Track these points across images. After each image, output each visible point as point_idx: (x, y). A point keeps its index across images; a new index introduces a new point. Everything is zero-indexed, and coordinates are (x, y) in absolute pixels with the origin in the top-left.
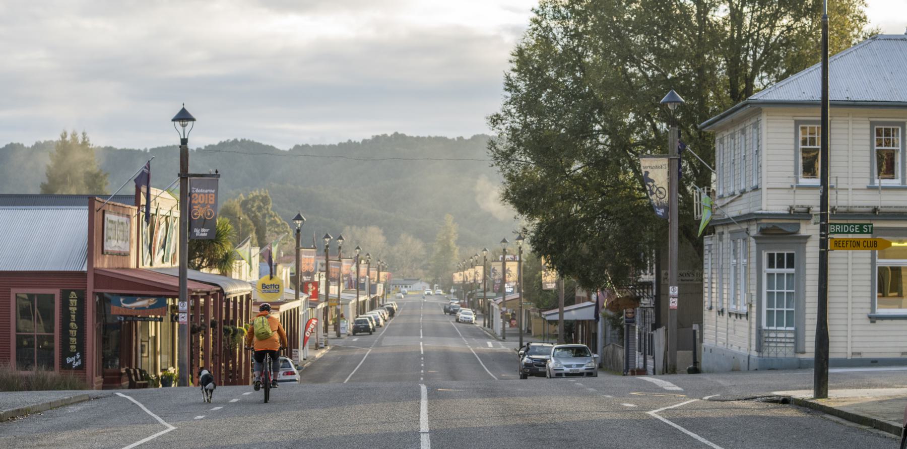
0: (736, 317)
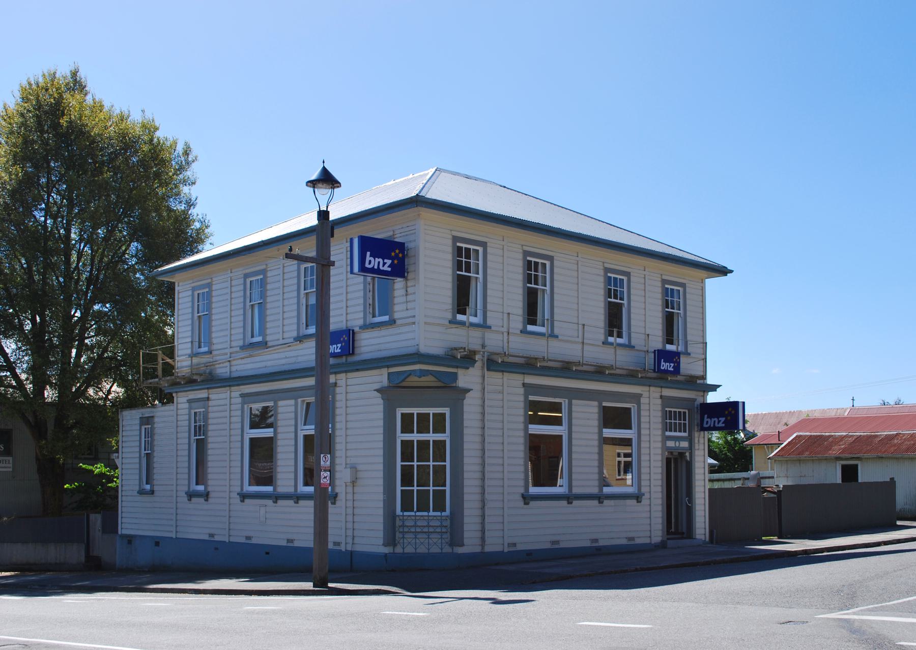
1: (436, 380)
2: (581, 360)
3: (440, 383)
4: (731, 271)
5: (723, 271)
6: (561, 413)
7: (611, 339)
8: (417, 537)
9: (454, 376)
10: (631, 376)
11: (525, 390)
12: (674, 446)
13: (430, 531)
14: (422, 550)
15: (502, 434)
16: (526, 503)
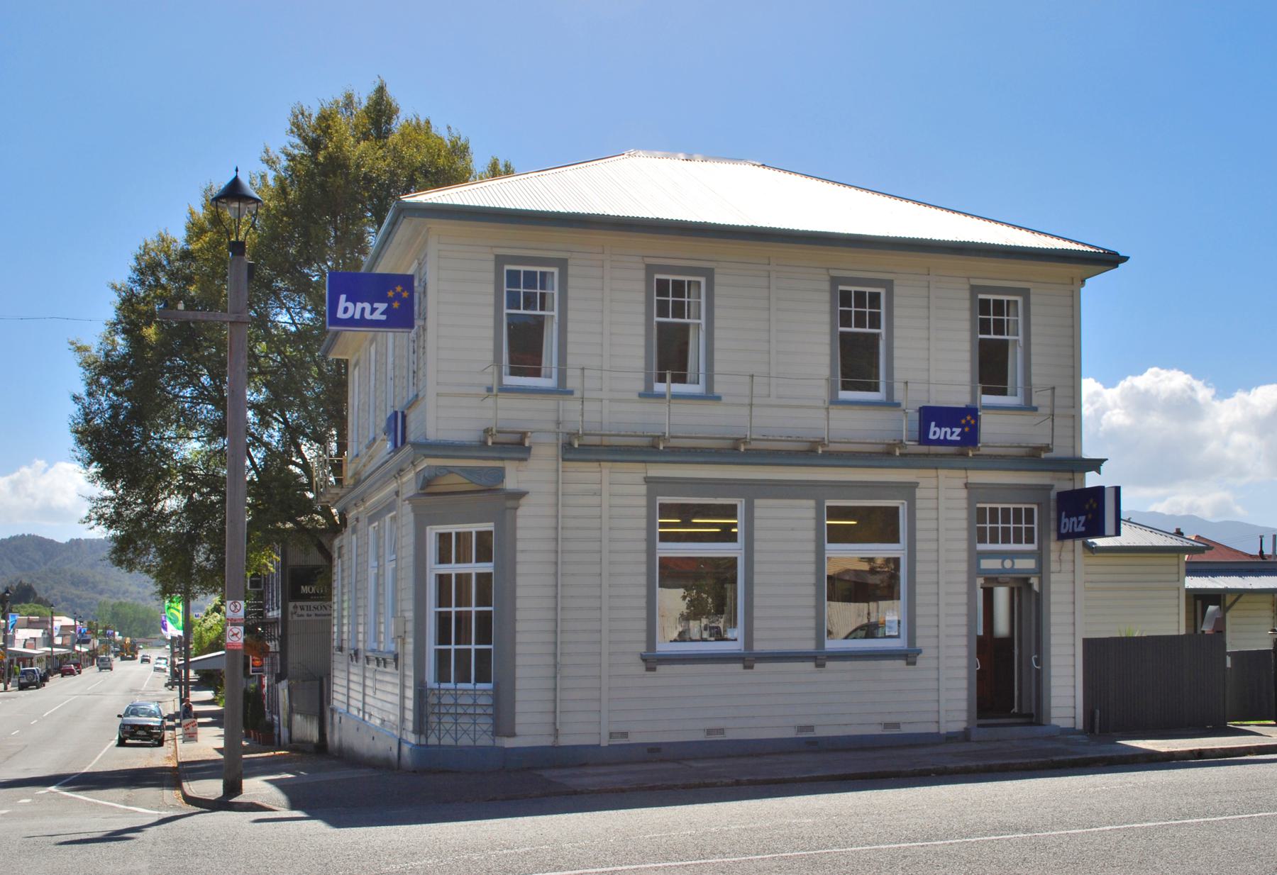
0: (378, 665)
1: (467, 481)
2: (748, 434)
3: (473, 485)
4: (1125, 259)
5: (1110, 260)
6: (736, 519)
7: (659, 387)
8: (477, 722)
9: (500, 474)
10: (886, 455)
11: (968, 492)
12: (1000, 567)
13: (477, 712)
14: (465, 741)
15: (599, 560)
16: (650, 669)
